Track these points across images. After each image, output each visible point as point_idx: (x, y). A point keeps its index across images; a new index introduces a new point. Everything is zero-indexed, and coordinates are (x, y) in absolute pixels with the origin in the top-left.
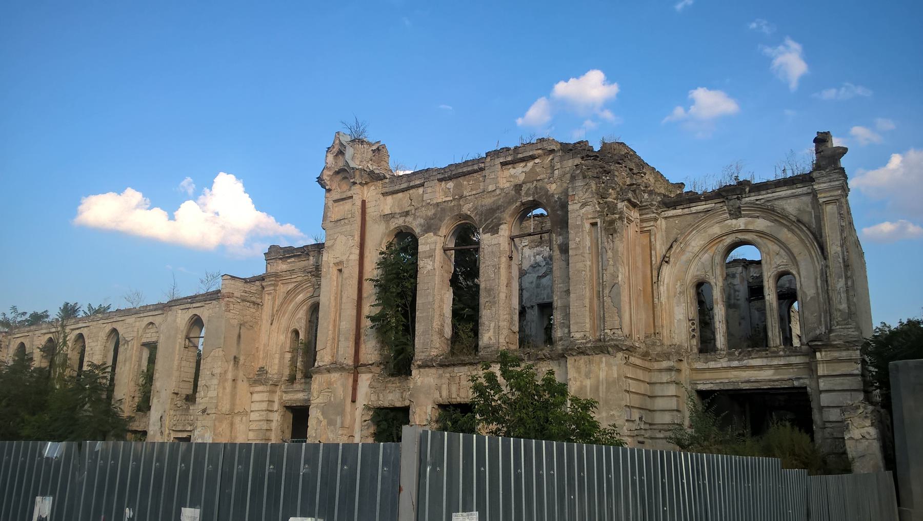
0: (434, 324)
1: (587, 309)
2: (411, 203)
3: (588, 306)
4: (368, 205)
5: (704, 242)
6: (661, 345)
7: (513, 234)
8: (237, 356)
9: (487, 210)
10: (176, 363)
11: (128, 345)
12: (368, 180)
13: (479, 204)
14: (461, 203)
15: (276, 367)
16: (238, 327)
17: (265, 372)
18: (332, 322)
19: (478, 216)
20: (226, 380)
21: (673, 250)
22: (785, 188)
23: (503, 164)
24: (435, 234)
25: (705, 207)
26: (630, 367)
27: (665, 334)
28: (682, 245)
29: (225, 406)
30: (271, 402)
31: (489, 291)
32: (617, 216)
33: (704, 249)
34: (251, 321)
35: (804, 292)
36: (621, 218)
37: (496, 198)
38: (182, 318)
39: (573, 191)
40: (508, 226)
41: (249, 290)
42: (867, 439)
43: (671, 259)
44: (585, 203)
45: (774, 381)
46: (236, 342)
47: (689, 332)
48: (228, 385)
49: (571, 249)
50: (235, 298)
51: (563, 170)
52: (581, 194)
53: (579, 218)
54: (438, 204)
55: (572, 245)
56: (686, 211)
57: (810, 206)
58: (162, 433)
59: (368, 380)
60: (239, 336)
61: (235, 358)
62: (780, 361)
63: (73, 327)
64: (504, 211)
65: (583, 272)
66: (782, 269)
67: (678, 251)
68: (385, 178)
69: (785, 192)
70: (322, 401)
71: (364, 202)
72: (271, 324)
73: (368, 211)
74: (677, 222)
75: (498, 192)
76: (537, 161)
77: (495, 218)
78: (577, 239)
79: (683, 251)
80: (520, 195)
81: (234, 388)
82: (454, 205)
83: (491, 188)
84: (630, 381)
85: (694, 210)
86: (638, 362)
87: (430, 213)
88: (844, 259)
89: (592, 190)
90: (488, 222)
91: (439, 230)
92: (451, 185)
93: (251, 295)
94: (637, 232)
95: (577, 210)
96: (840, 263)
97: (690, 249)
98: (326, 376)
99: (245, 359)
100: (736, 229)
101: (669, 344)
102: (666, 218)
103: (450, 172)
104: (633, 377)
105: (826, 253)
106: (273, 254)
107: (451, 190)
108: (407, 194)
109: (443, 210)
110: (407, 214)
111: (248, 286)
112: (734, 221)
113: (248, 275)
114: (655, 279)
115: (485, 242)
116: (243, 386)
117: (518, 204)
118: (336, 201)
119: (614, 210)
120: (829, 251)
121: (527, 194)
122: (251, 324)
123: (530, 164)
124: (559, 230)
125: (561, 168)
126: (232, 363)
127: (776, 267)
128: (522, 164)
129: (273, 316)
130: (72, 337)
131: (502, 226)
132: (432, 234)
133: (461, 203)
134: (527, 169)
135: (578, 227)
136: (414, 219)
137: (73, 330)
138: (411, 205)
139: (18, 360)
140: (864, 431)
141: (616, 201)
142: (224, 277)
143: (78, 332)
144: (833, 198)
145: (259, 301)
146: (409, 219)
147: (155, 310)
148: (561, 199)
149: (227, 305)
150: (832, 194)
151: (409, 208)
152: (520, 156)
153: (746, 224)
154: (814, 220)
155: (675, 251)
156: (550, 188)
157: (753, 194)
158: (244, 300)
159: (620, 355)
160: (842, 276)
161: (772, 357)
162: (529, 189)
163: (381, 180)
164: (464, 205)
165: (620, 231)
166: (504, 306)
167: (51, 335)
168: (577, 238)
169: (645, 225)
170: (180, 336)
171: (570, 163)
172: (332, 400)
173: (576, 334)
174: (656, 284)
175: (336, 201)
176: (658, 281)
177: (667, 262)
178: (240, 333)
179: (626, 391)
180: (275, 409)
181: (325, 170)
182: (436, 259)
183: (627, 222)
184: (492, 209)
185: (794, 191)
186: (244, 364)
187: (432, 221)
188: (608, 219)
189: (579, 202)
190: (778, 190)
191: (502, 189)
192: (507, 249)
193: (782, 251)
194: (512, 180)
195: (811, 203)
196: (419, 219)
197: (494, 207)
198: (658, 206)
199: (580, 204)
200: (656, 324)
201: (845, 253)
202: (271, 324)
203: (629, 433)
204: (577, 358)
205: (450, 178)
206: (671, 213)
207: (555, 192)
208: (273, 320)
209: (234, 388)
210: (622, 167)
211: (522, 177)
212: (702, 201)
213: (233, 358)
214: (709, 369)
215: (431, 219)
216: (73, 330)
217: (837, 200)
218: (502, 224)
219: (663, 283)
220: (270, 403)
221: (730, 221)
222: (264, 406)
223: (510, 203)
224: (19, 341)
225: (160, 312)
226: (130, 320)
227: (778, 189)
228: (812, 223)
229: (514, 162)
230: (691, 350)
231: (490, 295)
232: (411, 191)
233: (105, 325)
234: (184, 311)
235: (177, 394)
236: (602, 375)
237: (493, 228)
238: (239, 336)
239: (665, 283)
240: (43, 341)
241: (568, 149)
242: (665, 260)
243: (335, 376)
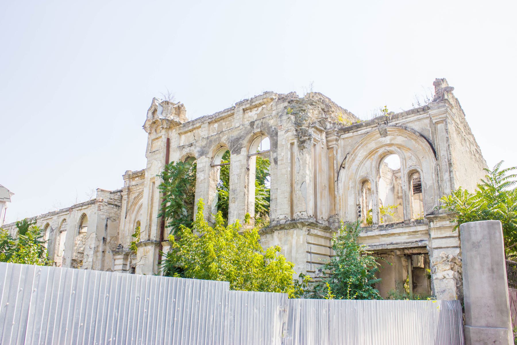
2: (195, 138)
5: (366, 153)
6: (338, 222)
8: (105, 237)
9: (234, 139)
11: (53, 232)
13: (231, 136)
14: (221, 136)
16: (106, 220)
17: (122, 247)
19: (230, 144)
21: (347, 159)
22: (413, 115)
24: (206, 157)
26: (313, 237)
27: (341, 215)
28: (353, 156)
30: (125, 265)
32: (307, 138)
33: (366, 157)
35: (425, 183)
36: (309, 139)
37: (240, 131)
38: (77, 215)
39: (281, 123)
40: (247, 149)
41: (114, 198)
42: (447, 279)
43: (346, 165)
44: (287, 131)
45: (407, 243)
46: (104, 229)
47: (357, 213)
48: (100, 254)
49: (279, 160)
50: (104, 203)
51: (278, 110)
52: (285, 124)
53: (284, 140)
55: (279, 158)
56: (355, 133)
57: (429, 126)
59: (167, 250)
60: (107, 225)
61: (104, 238)
62: (411, 229)
64: (244, 139)
65: (286, 175)
66: (413, 168)
67: (350, 160)
69: (413, 117)
70: (142, 263)
71: (168, 140)
72: (126, 218)
74: (350, 141)
76: (264, 106)
77: (239, 144)
79: (353, 160)
80: (253, 128)
81: (104, 256)
82: (217, 138)
84: (312, 246)
86: (320, 233)
87: (204, 143)
88: (448, 159)
89: (292, 122)
90: (235, 147)
91: (208, 154)
92: (216, 125)
93: (114, 201)
94: (323, 148)
95: (283, 135)
96: (446, 162)
97: (358, 158)
99: (111, 240)
100: (385, 143)
102: (343, 139)
103: (215, 117)
104: (315, 243)
105: (437, 156)
107: (216, 129)
108: (192, 133)
109: (211, 141)
110: (191, 145)
111: (113, 195)
112: (384, 139)
113: (113, 189)
114: (336, 179)
115: (233, 160)
116: (109, 255)
119: (305, 133)
120: (439, 155)
121: (257, 128)
122: (114, 218)
123: (260, 109)
124: (274, 149)
125: (277, 109)
126: (102, 241)
127: (409, 168)
128: (256, 109)
131: (242, 149)
132: (204, 157)
133: (221, 136)
134: (258, 112)
135: (283, 146)
136: (195, 148)
140: (445, 273)
141: (307, 129)
142: (98, 190)
144: (442, 119)
145: (119, 204)
146: (192, 148)
147: (66, 211)
148: (276, 129)
149: (99, 207)
150: (441, 116)
151: (193, 142)
153: (391, 140)
154: (431, 135)
155: (348, 160)
156: (270, 122)
157: (394, 120)
158: (109, 204)
159: (305, 228)
160: (447, 171)
161: (405, 227)
162: (258, 124)
163: (178, 125)
164: (222, 137)
165: (307, 147)
166: (242, 200)
168: (282, 153)
171: (282, 105)
172: (147, 262)
173: (280, 216)
174: (336, 182)
176: (337, 180)
177: (344, 168)
178: (107, 223)
179: (307, 252)
181: (147, 122)
182: (206, 172)
183: (314, 141)
184: (237, 138)
185: (418, 116)
186: (110, 242)
187: (204, 149)
188: (302, 139)
189: (284, 130)
190: (408, 117)
192: (245, 164)
193: (413, 156)
194: (250, 119)
195: (429, 124)
196: (198, 148)
197: (239, 137)
199: (284, 131)
200: (336, 208)
201: (449, 155)
202: (126, 218)
204: (280, 232)
207: (273, 125)
208: (126, 216)
209: (104, 256)
210: (315, 107)
211: (255, 117)
213: (102, 239)
214: (368, 237)
215: (204, 147)
217: (444, 120)
218: (242, 148)
219: (341, 182)
220: (124, 266)
221: (381, 138)
223: (247, 134)
225: (68, 212)
226: (55, 217)
227: (409, 116)
228: (430, 137)
229: (250, 109)
231: (234, 193)
233: (43, 221)
234: (79, 211)
237: (237, 150)
238: (107, 225)
241: (282, 98)
242: (342, 167)
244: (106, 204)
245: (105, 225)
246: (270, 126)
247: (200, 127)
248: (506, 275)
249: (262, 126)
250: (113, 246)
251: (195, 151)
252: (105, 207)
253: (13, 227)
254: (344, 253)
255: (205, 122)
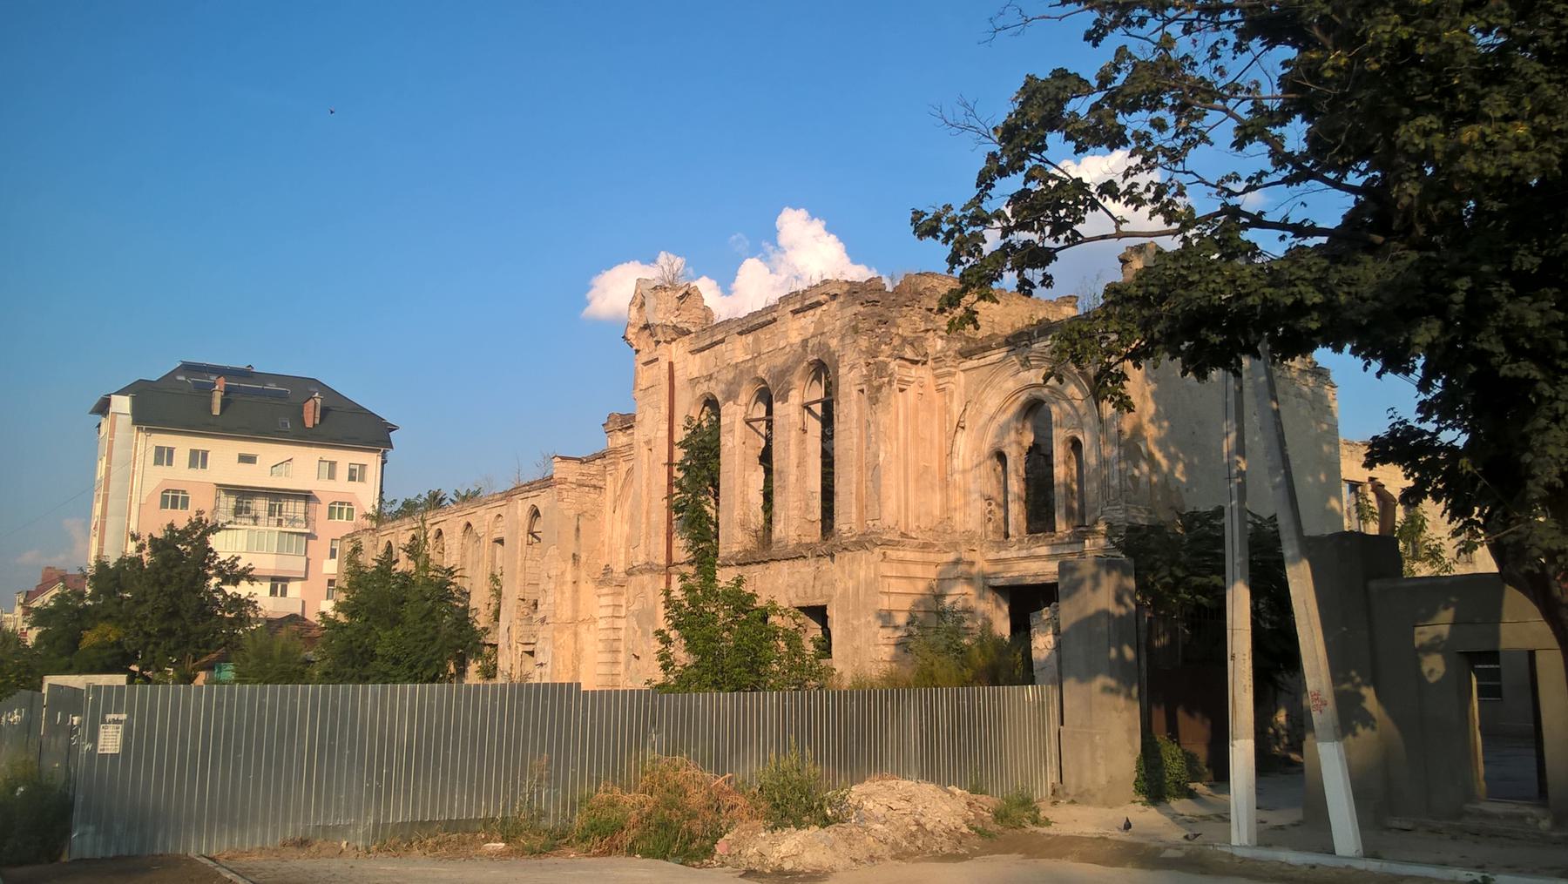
0: (736, 513)
1: (854, 496)
3: (854, 491)
4: (676, 367)
7: (806, 401)
10: (519, 563)
12: (674, 336)
15: (622, 564)
18: (644, 514)
20: (564, 583)
21: (967, 412)
23: (795, 312)
25: (998, 356)
29: (566, 613)
31: (780, 473)
32: (886, 380)
34: (592, 510)
36: (890, 383)
37: (787, 356)
46: (574, 539)
48: (568, 588)
54: (737, 365)
58: (510, 647)
60: (578, 529)
61: (574, 555)
63: (433, 521)
68: (689, 332)
71: (671, 365)
73: (676, 374)
75: (788, 349)
76: (825, 307)
78: (846, 411)
81: (576, 591)
83: (782, 344)
85: (988, 360)
92: (750, 338)
98: (640, 577)
101: (963, 530)
106: (611, 425)
109: (741, 372)
117: (805, 364)
118: (646, 364)
123: (819, 311)
126: (571, 561)
128: (812, 312)
129: (615, 502)
130: (432, 533)
131: (791, 393)
132: (731, 403)
136: (717, 385)
137: (432, 524)
138: (716, 365)
139: (1329, 241)
143: (436, 527)
145: (601, 484)
146: (713, 383)
149: (559, 493)
152: (807, 302)
157: (1041, 339)
167: (413, 532)
169: (940, 381)
170: (521, 532)
175: (646, 364)
177: (963, 428)
180: (623, 615)
188: (875, 384)
191: (791, 346)
198: (955, 357)
203: (885, 641)
205: (749, 331)
206: (969, 364)
209: (576, 591)
212: (994, 349)
215: (732, 384)
216: (432, 524)
222: (609, 611)
224: (386, 539)
230: (986, 536)
232: (717, 347)
235: (523, 600)
236: (862, 574)
238: (578, 529)
239: (961, 454)
240: (406, 539)
243: (646, 578)
244: (574, 486)
245: (574, 529)
246: (832, 350)
247: (722, 341)
248: (1248, 627)
249: (820, 350)
250: (594, 570)
251: (718, 391)
252: (574, 494)
253: (400, 529)
254: (243, 589)
255: (732, 332)
